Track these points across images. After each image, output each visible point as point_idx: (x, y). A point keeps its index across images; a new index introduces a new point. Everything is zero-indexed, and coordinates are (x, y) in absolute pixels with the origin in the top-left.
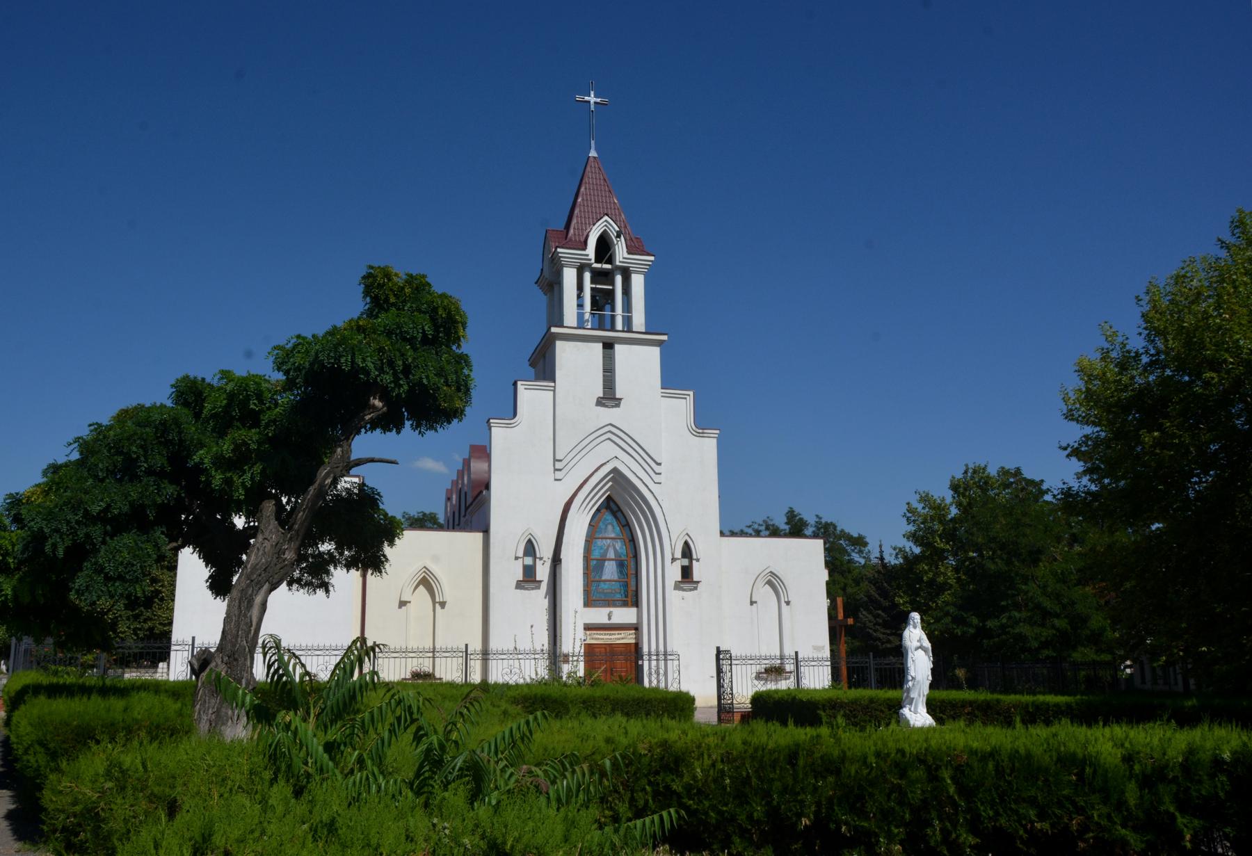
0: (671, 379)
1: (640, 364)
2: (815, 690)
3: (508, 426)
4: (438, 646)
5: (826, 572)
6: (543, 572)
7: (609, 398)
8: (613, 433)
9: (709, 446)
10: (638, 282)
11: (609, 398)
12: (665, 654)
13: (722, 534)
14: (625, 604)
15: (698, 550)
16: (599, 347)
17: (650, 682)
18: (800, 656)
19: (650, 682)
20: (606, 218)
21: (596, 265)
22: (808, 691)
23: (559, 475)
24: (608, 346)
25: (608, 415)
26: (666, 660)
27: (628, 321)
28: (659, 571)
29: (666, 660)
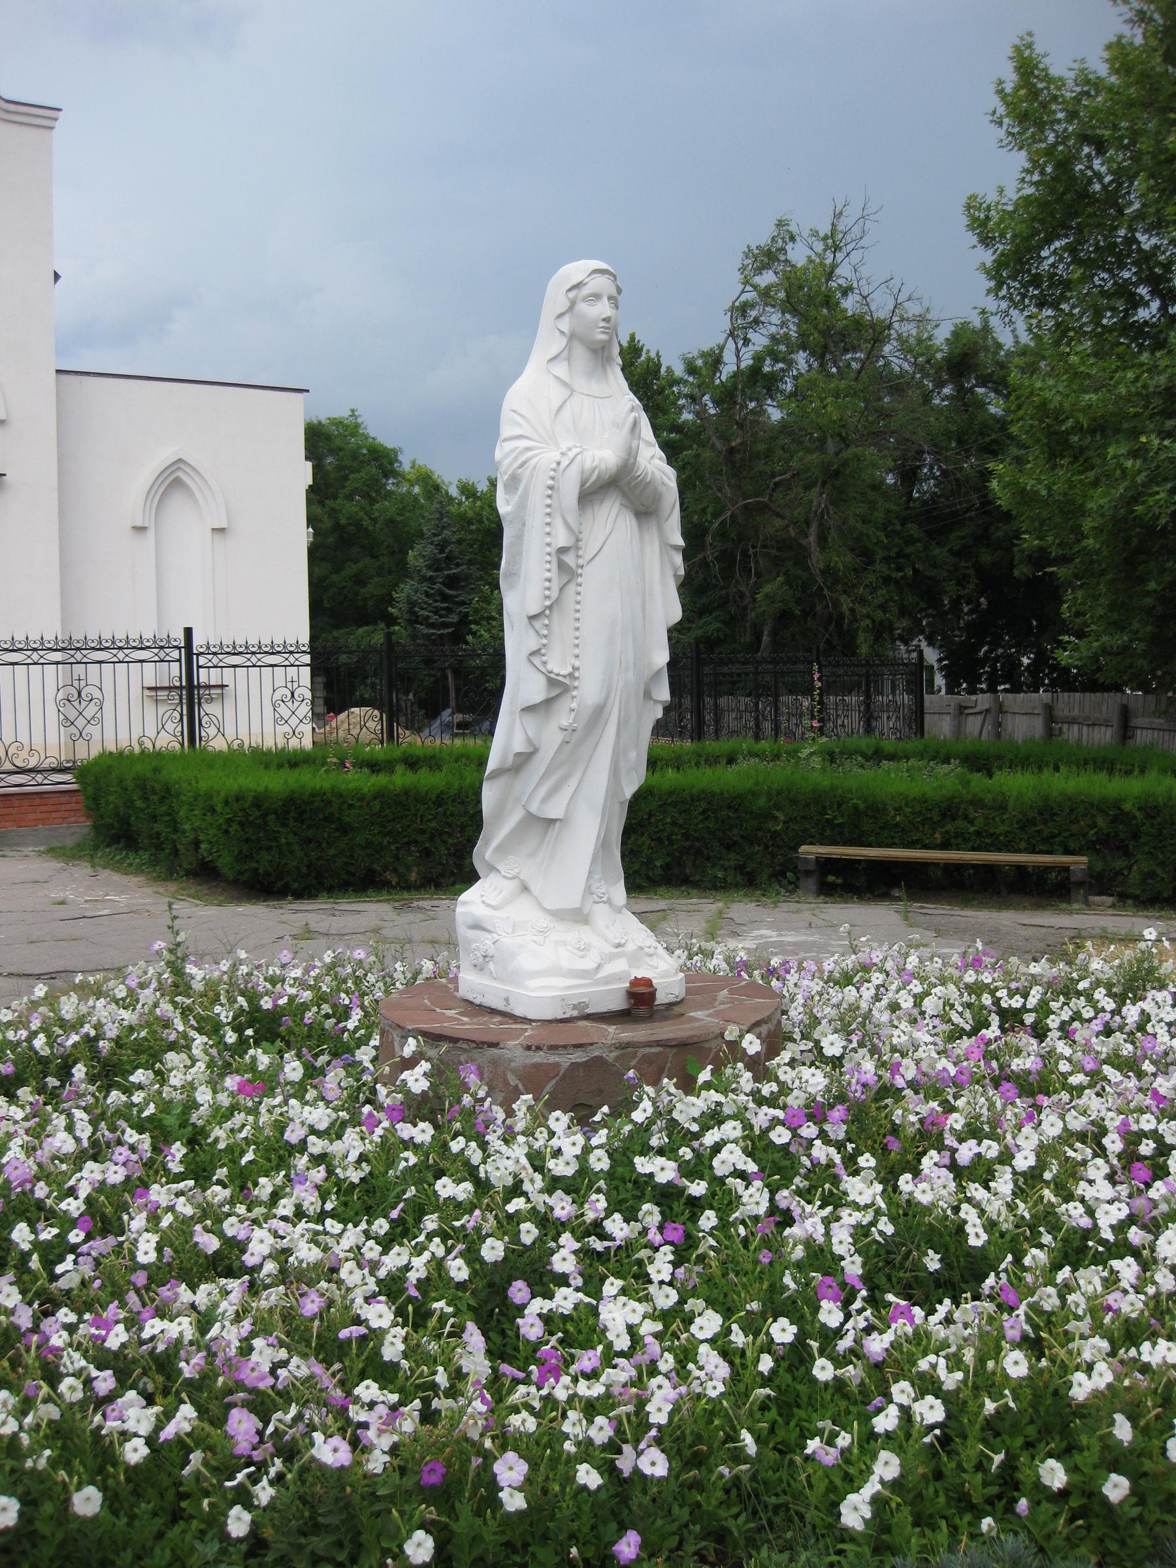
18: (198, 641)
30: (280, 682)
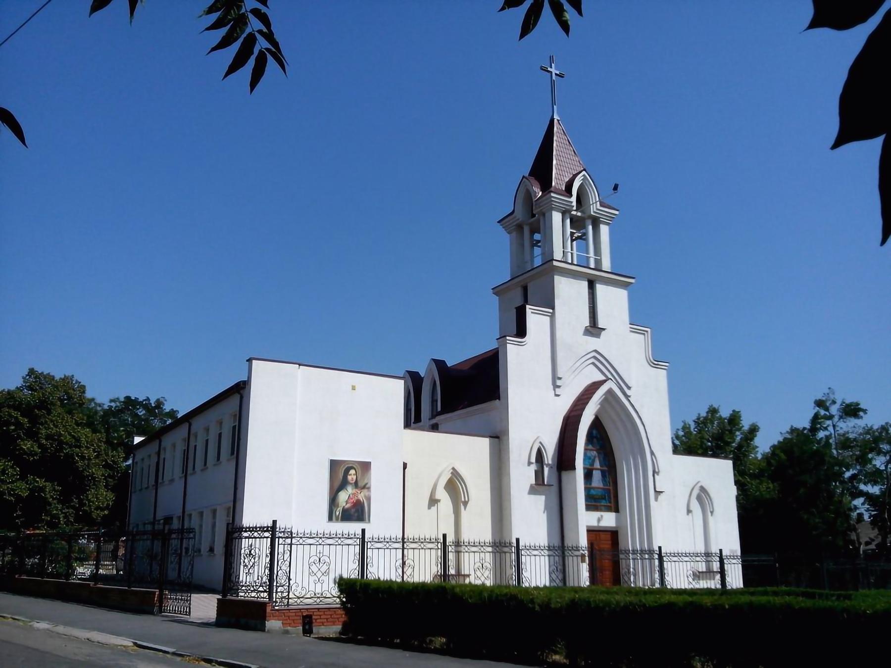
0: (638, 319)
1: (614, 302)
2: (537, 588)
3: (520, 344)
4: (409, 534)
5: (735, 488)
7: (594, 328)
8: (598, 359)
9: (661, 375)
10: (604, 230)
11: (594, 328)
12: (458, 544)
13: (676, 450)
14: (608, 509)
16: (585, 284)
17: (635, 582)
19: (635, 582)
20: (584, 172)
21: (574, 213)
22: (527, 589)
23: (558, 391)
25: (592, 343)
26: (458, 552)
27: (598, 262)
29: (458, 552)
30: (313, 553)
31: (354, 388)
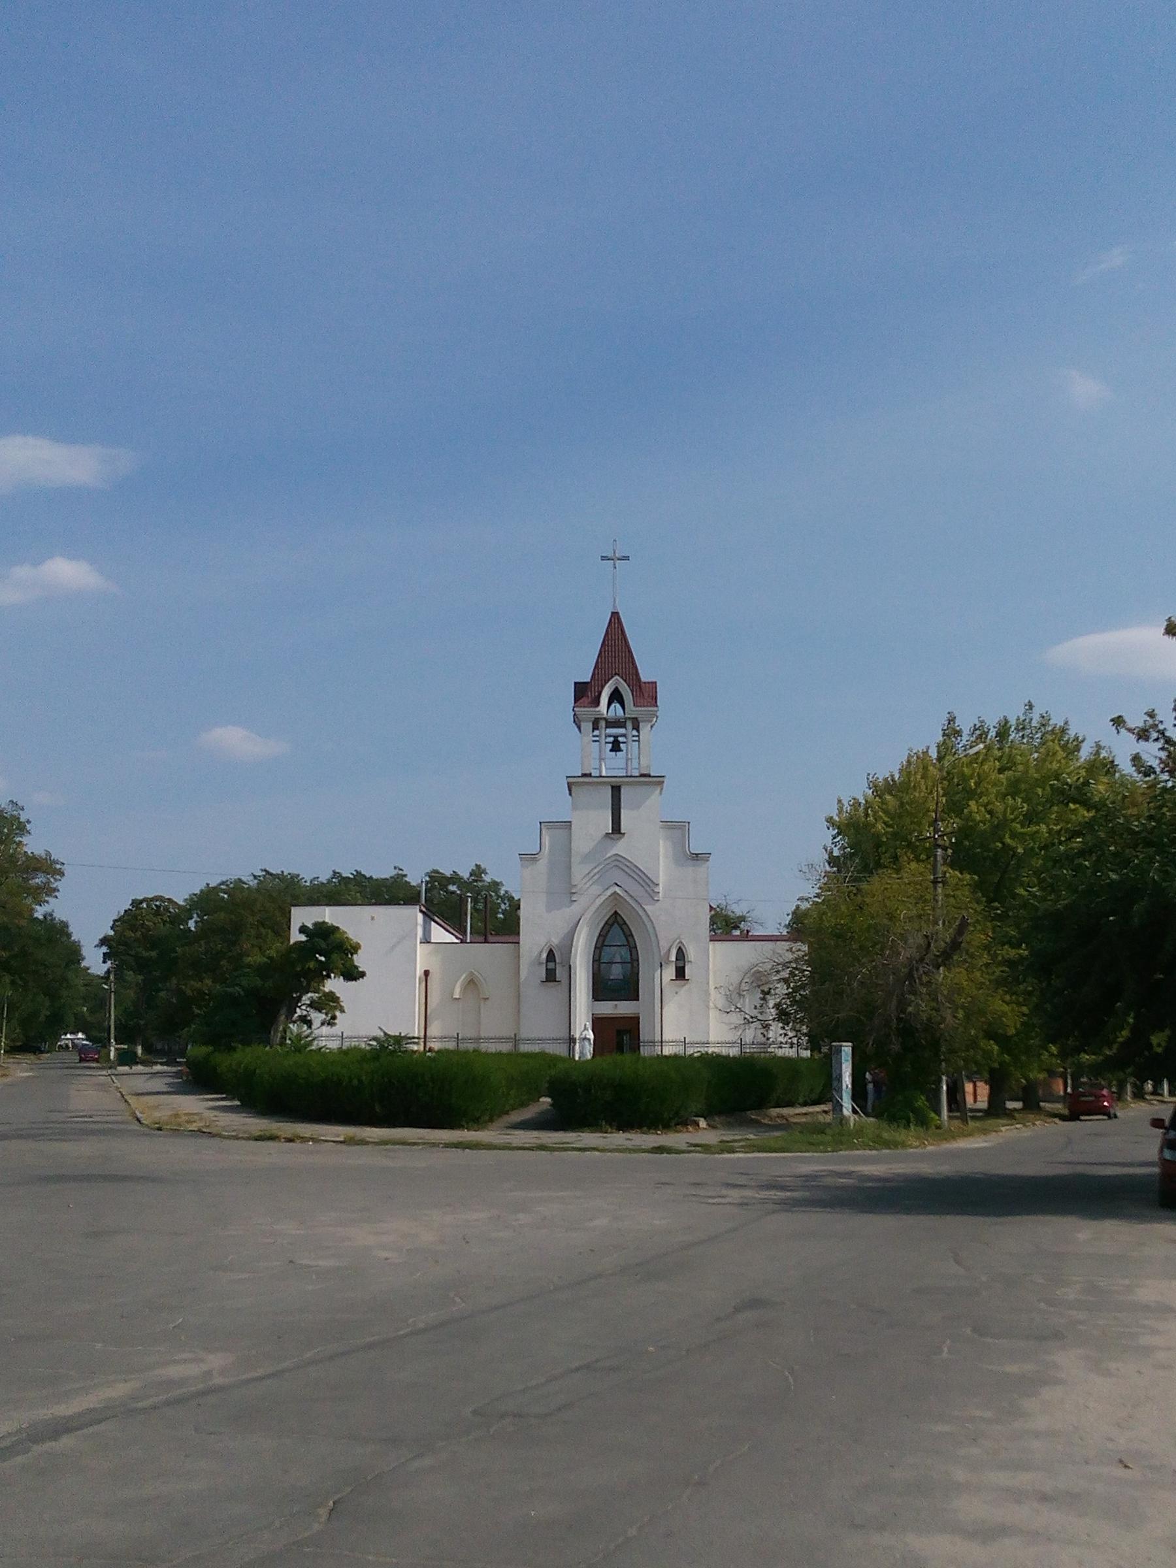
6: (560, 973)
7: (617, 828)
8: (619, 862)
11: (617, 828)
15: (691, 953)
24: (616, 790)
28: (657, 977)
31: (373, 918)
